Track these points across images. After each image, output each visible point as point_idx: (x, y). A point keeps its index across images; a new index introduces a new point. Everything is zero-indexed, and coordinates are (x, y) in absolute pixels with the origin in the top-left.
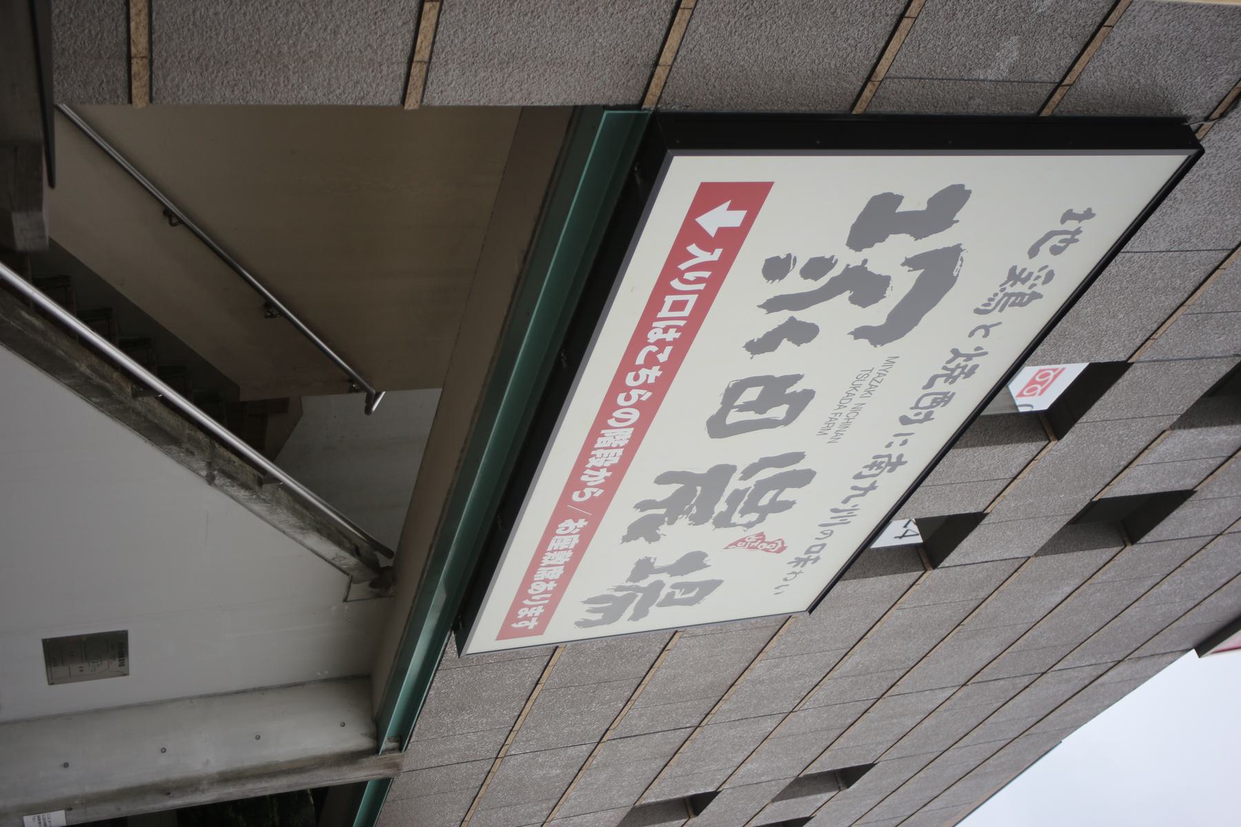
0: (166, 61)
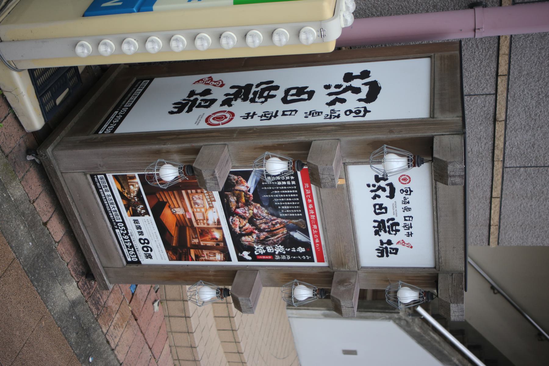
0: (506, 227)
